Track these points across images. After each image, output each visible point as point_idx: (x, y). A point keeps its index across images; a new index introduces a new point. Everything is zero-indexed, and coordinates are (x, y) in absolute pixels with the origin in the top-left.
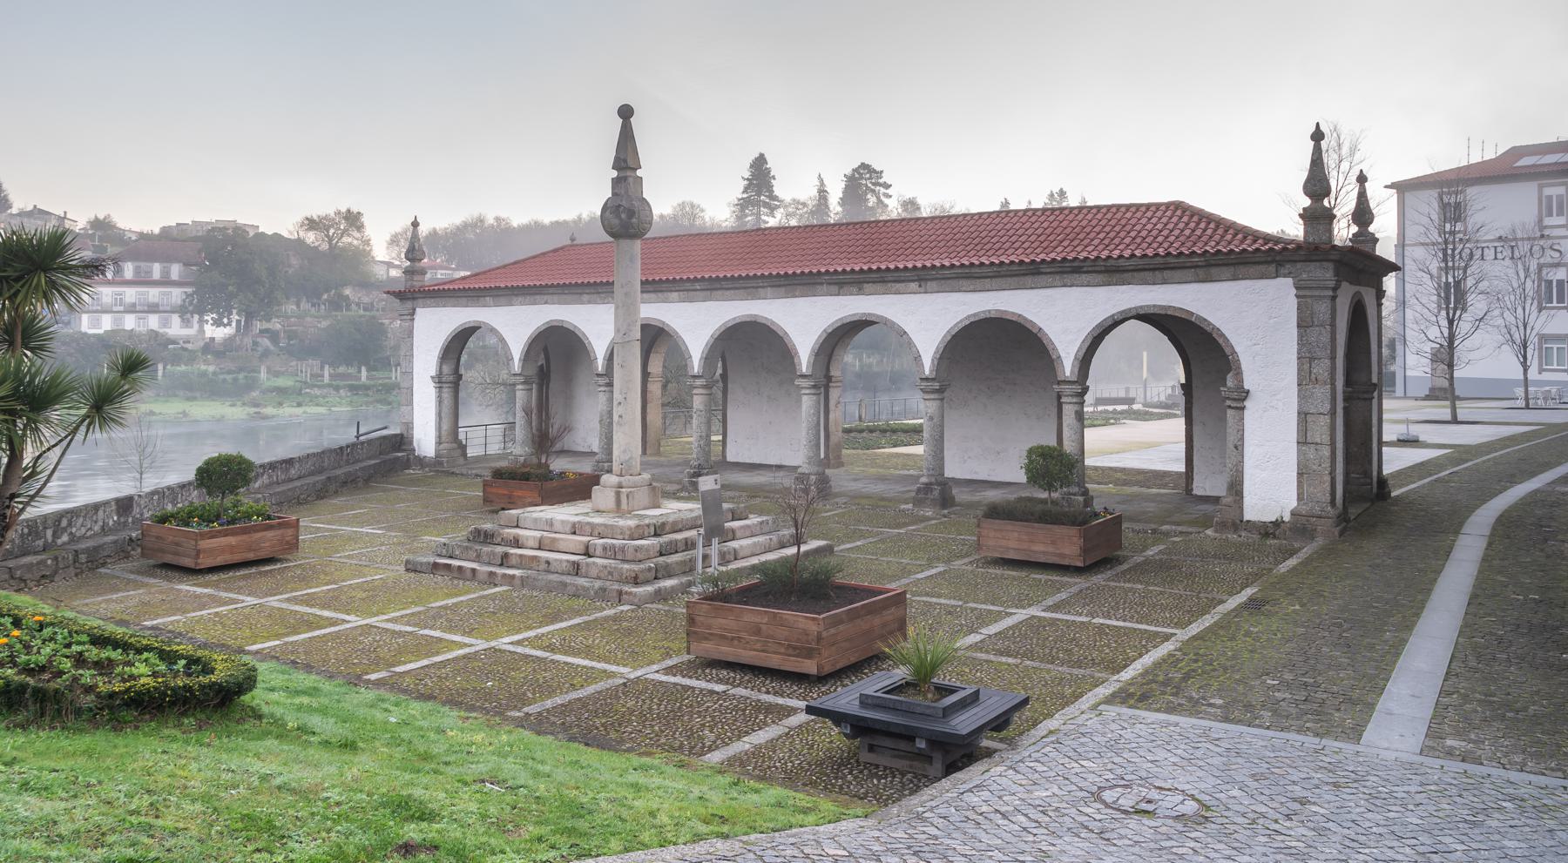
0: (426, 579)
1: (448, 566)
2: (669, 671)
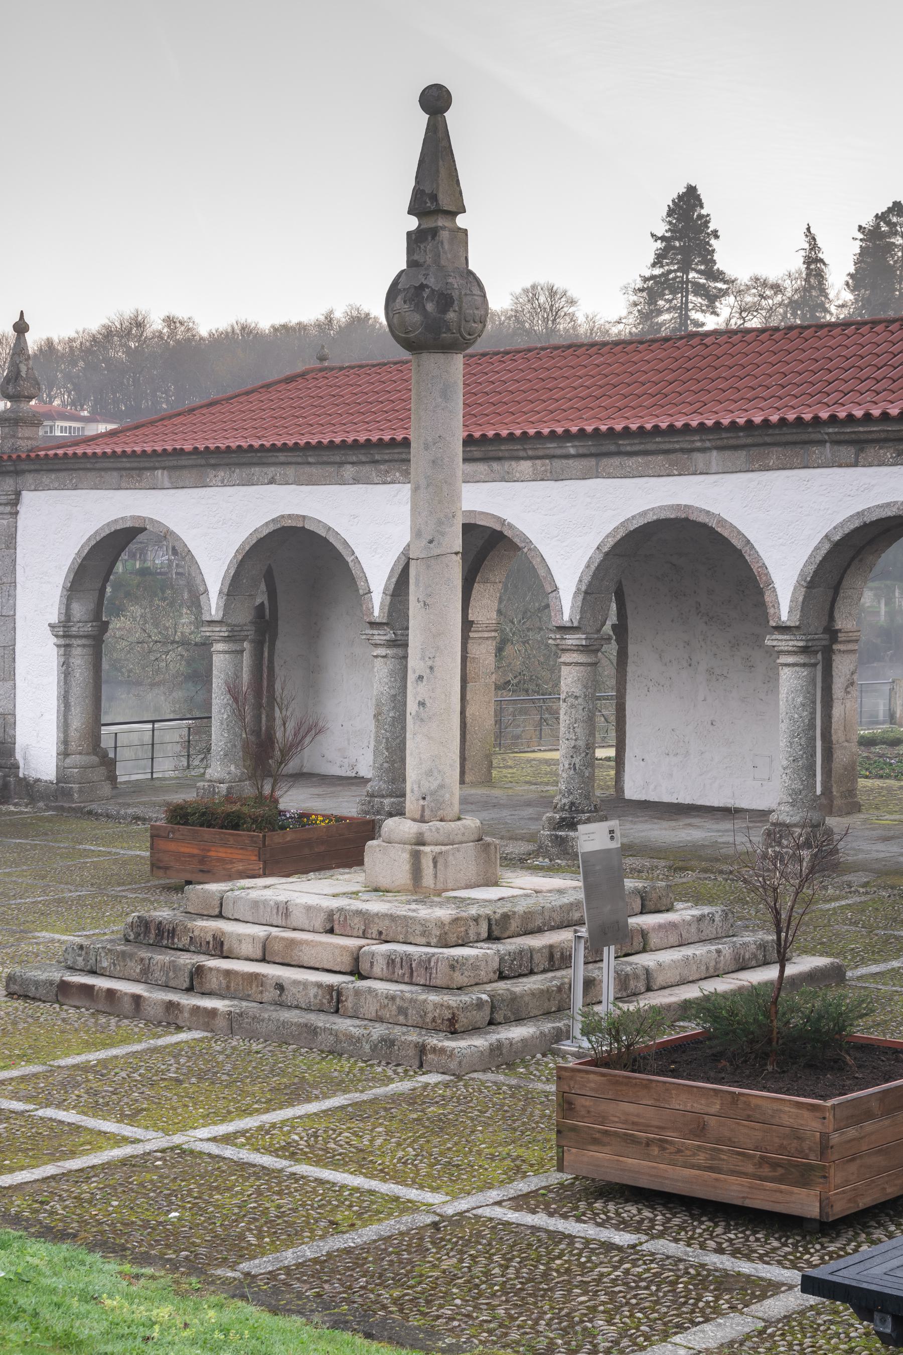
0: (46, 1011)
1: (88, 990)
2: (520, 1202)
